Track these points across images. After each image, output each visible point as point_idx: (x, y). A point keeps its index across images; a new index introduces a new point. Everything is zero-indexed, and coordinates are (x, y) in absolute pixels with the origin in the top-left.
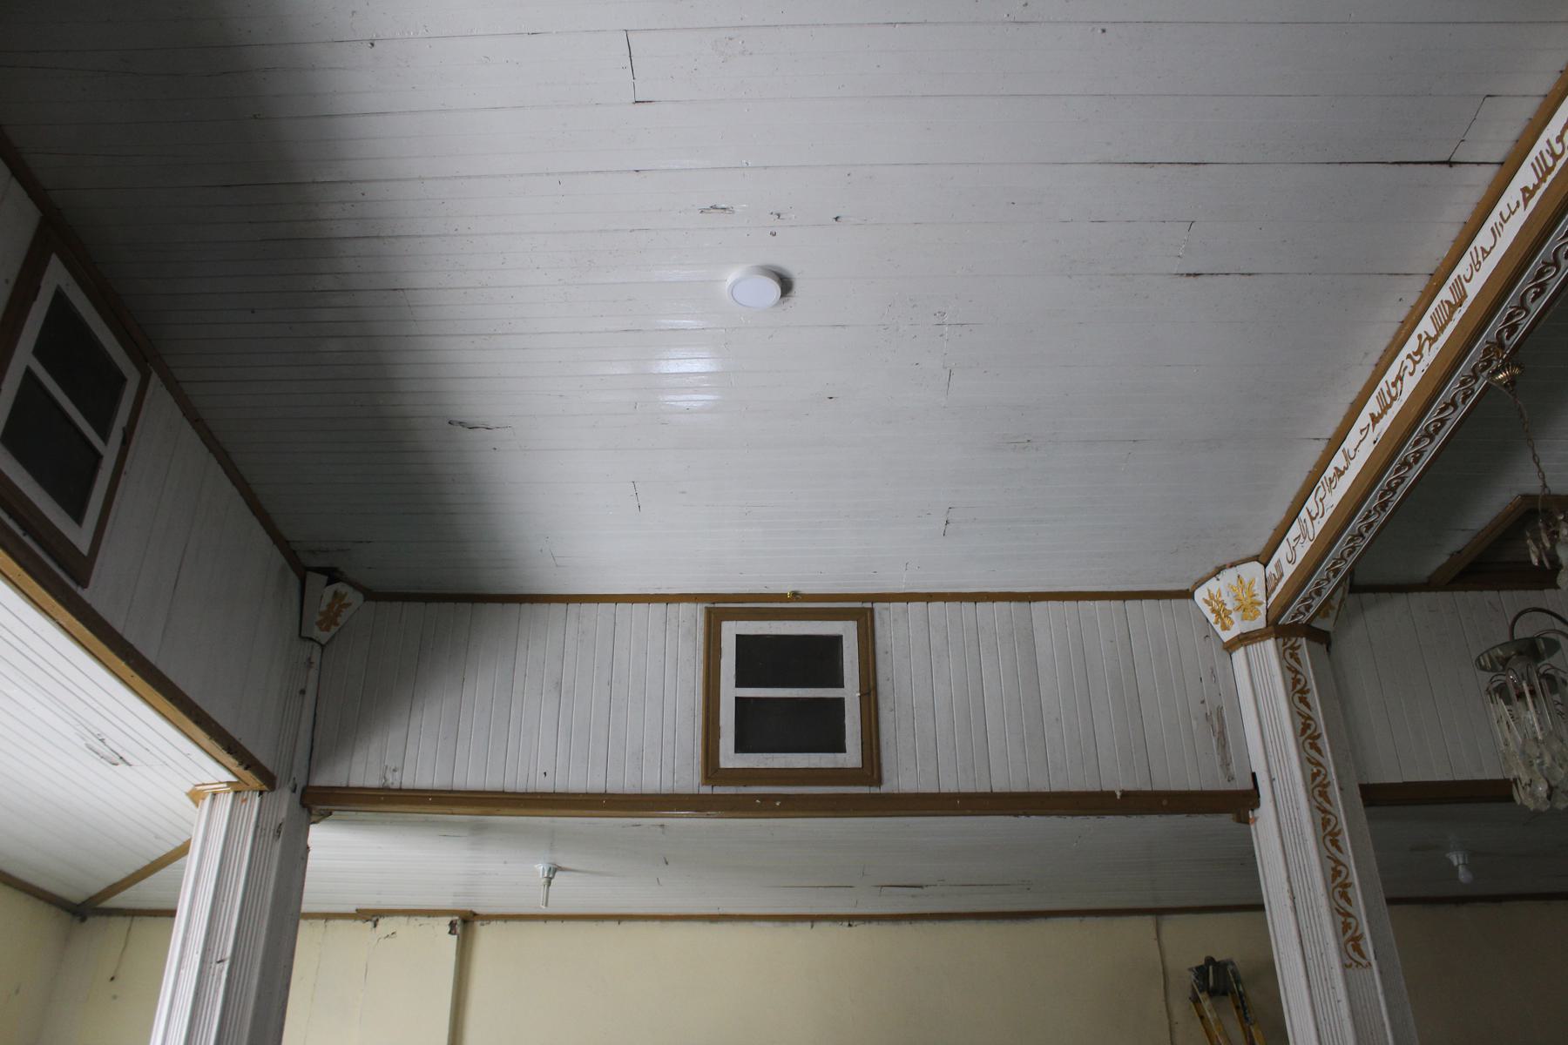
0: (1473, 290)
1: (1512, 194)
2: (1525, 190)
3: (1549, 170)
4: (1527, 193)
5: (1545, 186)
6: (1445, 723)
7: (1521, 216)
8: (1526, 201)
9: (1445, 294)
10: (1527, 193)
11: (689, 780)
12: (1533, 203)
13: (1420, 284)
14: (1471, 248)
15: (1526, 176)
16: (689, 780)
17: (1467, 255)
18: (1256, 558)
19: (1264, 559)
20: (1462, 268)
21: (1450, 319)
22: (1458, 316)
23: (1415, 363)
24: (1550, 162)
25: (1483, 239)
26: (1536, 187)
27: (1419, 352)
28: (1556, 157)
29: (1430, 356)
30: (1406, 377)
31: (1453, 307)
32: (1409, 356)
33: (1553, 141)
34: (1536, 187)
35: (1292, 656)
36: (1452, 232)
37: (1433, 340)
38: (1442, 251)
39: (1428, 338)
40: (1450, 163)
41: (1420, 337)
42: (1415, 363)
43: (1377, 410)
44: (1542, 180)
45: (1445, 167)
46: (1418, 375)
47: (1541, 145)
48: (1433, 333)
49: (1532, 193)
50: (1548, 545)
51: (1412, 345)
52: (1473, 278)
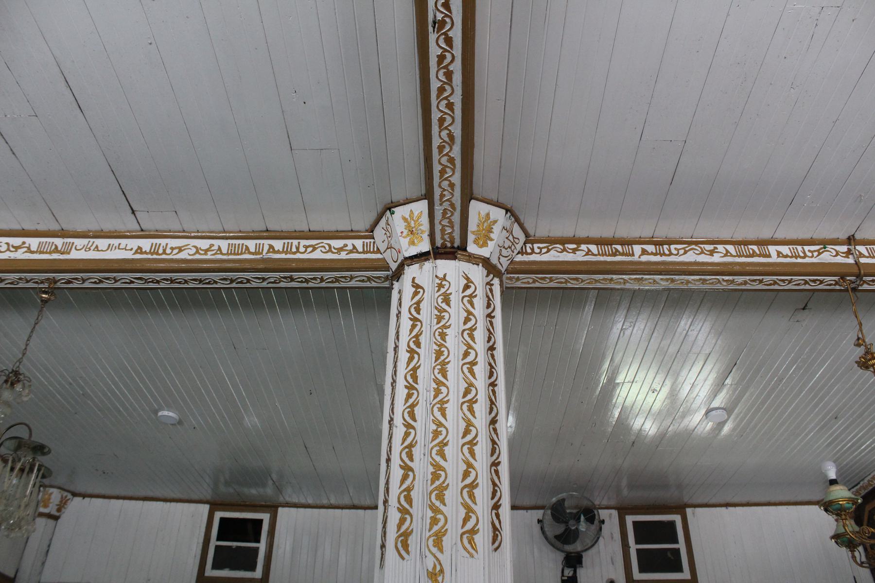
0: (74, 255)
1: (134, 243)
2: (140, 248)
3: (157, 254)
4: (139, 250)
5: (149, 256)
6: (872, 542)
7: (129, 255)
8: (136, 252)
9: (59, 242)
10: (139, 250)
11: (689, 511)
12: (138, 256)
13: (55, 227)
14: (92, 240)
15: (146, 244)
16: (689, 511)
17: (88, 240)
18: (527, 235)
19: (529, 239)
20: (79, 242)
21: (50, 253)
22: (55, 256)
23: (8, 250)
24: (161, 251)
25: (102, 243)
26: (146, 253)
27: (17, 248)
28: (164, 252)
29: (20, 255)
30: (21, 251)
31: (56, 250)
32: (8, 244)
33: (169, 246)
34: (146, 253)
35: (440, 409)
36: (94, 227)
37: (29, 250)
38: (80, 228)
39: (29, 248)
40: (133, 212)
41: (24, 243)
42: (8, 250)
43: (34, 248)
44: (151, 253)
45: (131, 211)
46: (348, 257)
47: (163, 242)
48: (224, 251)
49: (142, 253)
50: (848, 278)
51: (16, 241)
52: (81, 251)
